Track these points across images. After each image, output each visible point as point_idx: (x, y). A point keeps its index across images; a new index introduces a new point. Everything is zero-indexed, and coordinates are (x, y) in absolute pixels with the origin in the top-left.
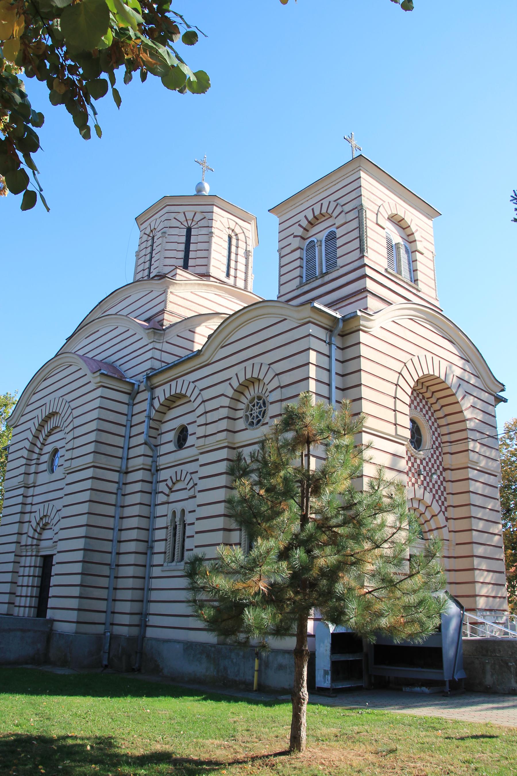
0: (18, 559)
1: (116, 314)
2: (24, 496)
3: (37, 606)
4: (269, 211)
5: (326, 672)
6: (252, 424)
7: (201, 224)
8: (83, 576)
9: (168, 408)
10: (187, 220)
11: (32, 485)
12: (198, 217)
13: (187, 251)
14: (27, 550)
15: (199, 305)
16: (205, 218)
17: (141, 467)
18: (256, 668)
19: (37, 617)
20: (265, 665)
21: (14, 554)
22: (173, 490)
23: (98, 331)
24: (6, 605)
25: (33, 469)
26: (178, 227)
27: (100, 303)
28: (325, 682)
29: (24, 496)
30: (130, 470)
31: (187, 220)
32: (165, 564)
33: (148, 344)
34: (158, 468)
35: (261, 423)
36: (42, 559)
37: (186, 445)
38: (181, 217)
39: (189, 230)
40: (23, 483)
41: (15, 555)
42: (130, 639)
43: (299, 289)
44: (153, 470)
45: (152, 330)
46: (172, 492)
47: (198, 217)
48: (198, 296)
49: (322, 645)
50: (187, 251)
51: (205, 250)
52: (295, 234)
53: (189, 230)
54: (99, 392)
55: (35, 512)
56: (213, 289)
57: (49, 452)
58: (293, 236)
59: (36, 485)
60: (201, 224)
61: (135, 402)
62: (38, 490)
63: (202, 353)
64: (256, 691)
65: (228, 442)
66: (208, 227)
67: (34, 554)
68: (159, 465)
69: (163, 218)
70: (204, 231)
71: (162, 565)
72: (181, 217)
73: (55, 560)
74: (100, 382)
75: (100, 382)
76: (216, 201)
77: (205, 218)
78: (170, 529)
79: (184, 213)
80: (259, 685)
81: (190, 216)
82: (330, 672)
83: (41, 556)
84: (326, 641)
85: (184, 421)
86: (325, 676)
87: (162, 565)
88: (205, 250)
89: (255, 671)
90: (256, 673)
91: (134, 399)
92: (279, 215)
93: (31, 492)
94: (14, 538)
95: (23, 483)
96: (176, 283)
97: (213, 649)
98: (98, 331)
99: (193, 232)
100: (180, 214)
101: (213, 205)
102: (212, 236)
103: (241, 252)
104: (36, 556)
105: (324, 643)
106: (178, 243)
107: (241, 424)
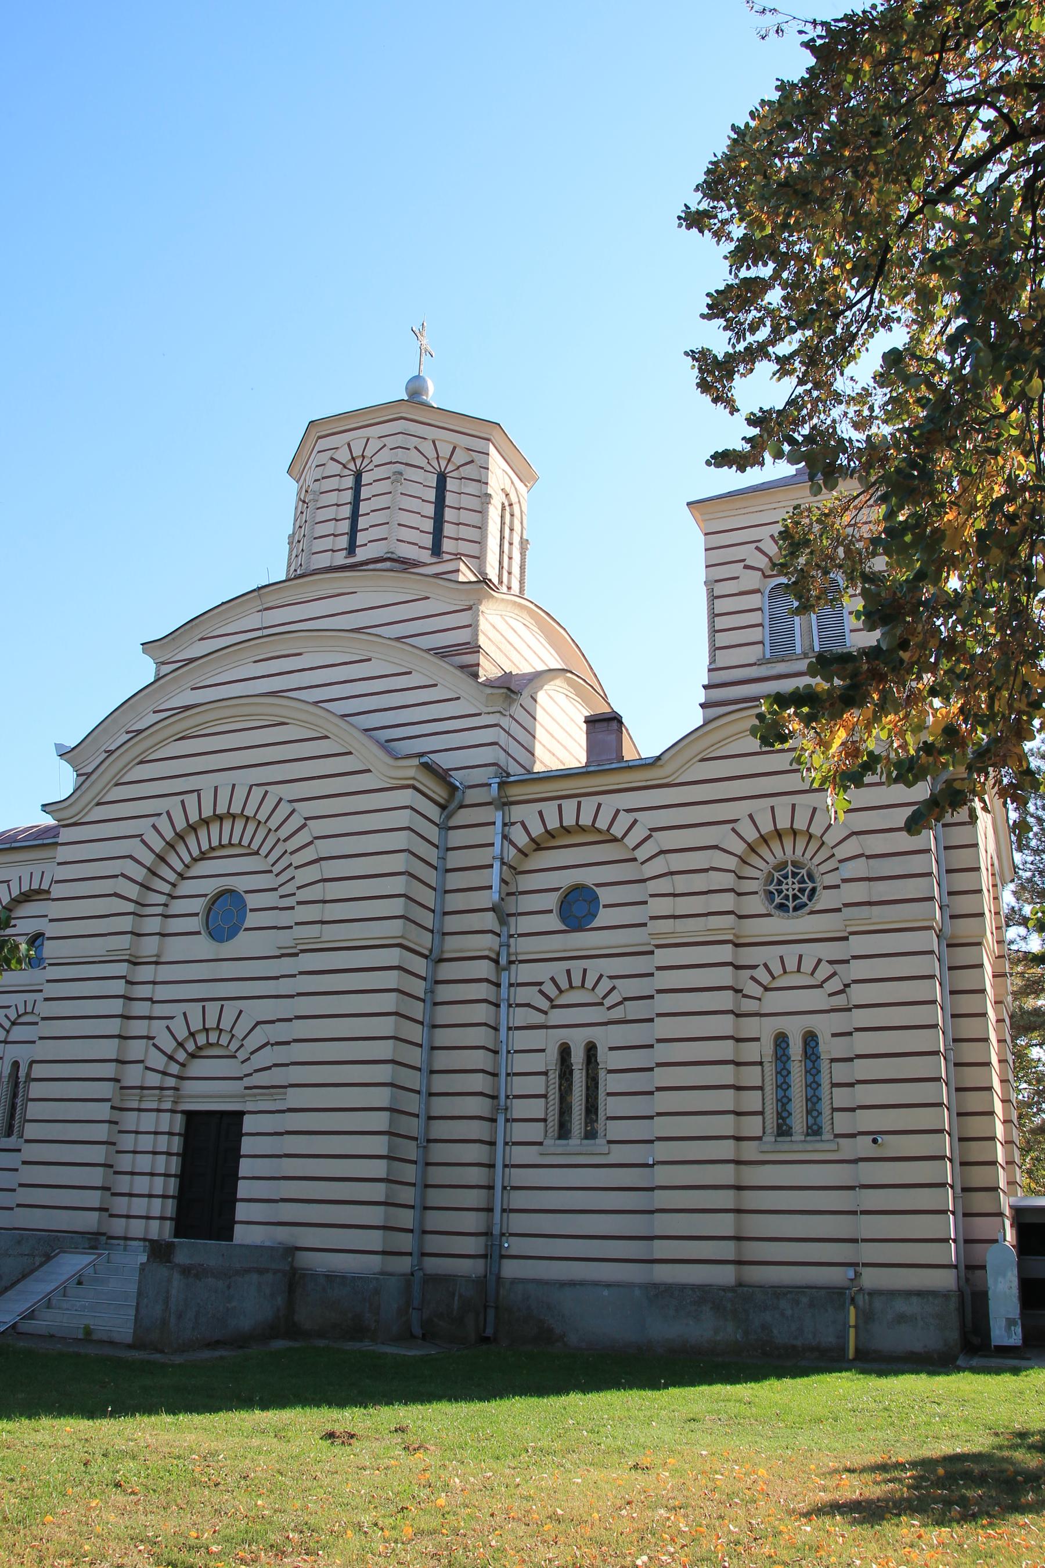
0: (117, 1115)
1: (398, 639)
2: (128, 982)
3: (174, 1216)
4: (688, 504)
5: (1010, 1322)
6: (782, 907)
7: (465, 471)
8: (391, 1161)
9: (535, 846)
10: (449, 460)
11: (153, 959)
12: (460, 458)
13: (439, 520)
14: (141, 1097)
15: (509, 642)
16: (472, 461)
17: (486, 953)
18: (852, 1322)
19: (176, 1236)
20: (867, 1317)
21: (109, 1104)
22: (555, 1003)
23: (300, 654)
24: (96, 1214)
25: (153, 925)
26: (422, 468)
27: (259, 588)
28: (1010, 1337)
29: (128, 982)
30: (447, 956)
31: (449, 460)
32: (548, 1142)
33: (479, 714)
34: (513, 958)
35: (807, 909)
36: (185, 1117)
37: (593, 925)
38: (428, 448)
39: (442, 479)
40: (128, 952)
41: (113, 1108)
42: (481, 1283)
43: (764, 667)
44: (503, 961)
45: (505, 691)
46: (553, 1007)
47: (460, 458)
48: (507, 623)
49: (1000, 1279)
50: (439, 520)
51: (473, 526)
52: (747, 563)
53: (442, 479)
54: (406, 797)
55: (9, 1007)
56: (525, 615)
57: (205, 895)
58: (742, 564)
59: (163, 960)
60: (465, 471)
61: (451, 824)
62: (165, 973)
63: (660, 763)
64: (854, 1360)
65: (735, 935)
66: (479, 481)
67: (168, 1106)
68: (516, 954)
69: (391, 442)
70: (472, 488)
71: (540, 1144)
72: (428, 448)
73: (249, 1124)
74: (414, 778)
75: (414, 778)
76: (496, 436)
77: (472, 461)
78: (554, 1077)
79: (434, 442)
80: (857, 1350)
81: (445, 451)
82: (1019, 1322)
83: (183, 1112)
84: (1009, 1274)
85: (588, 877)
86: (1010, 1329)
87: (540, 1144)
88: (473, 526)
89: (850, 1327)
90: (852, 1331)
91: (449, 817)
92: (707, 517)
93: (145, 973)
94: (108, 1070)
95: (128, 952)
96: (493, 596)
97: (730, 1295)
98: (300, 654)
99: (451, 484)
100: (426, 443)
101: (488, 440)
102: (489, 503)
103: (516, 540)
104: (173, 1111)
105: (1004, 1276)
106: (423, 500)
107: (756, 904)
